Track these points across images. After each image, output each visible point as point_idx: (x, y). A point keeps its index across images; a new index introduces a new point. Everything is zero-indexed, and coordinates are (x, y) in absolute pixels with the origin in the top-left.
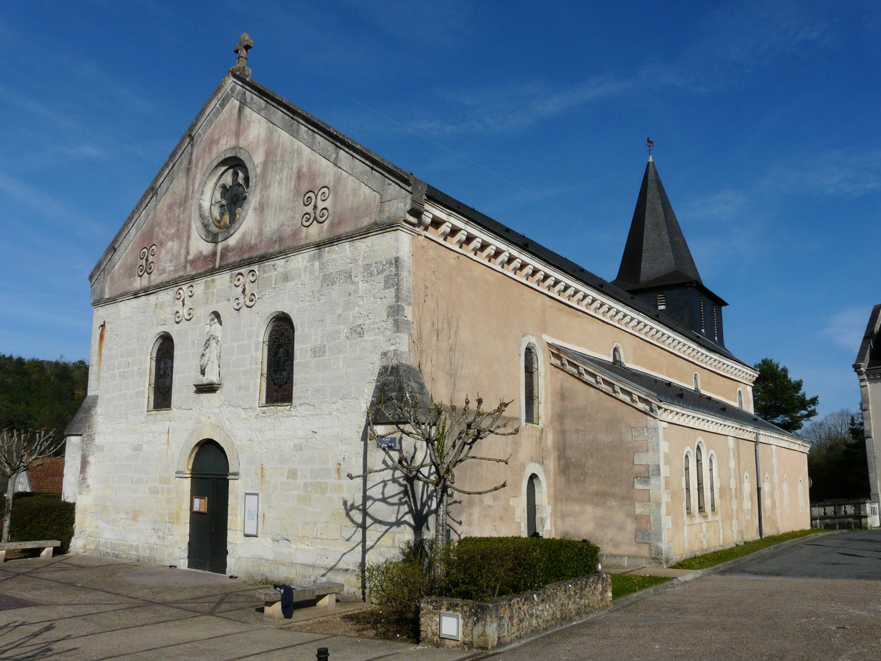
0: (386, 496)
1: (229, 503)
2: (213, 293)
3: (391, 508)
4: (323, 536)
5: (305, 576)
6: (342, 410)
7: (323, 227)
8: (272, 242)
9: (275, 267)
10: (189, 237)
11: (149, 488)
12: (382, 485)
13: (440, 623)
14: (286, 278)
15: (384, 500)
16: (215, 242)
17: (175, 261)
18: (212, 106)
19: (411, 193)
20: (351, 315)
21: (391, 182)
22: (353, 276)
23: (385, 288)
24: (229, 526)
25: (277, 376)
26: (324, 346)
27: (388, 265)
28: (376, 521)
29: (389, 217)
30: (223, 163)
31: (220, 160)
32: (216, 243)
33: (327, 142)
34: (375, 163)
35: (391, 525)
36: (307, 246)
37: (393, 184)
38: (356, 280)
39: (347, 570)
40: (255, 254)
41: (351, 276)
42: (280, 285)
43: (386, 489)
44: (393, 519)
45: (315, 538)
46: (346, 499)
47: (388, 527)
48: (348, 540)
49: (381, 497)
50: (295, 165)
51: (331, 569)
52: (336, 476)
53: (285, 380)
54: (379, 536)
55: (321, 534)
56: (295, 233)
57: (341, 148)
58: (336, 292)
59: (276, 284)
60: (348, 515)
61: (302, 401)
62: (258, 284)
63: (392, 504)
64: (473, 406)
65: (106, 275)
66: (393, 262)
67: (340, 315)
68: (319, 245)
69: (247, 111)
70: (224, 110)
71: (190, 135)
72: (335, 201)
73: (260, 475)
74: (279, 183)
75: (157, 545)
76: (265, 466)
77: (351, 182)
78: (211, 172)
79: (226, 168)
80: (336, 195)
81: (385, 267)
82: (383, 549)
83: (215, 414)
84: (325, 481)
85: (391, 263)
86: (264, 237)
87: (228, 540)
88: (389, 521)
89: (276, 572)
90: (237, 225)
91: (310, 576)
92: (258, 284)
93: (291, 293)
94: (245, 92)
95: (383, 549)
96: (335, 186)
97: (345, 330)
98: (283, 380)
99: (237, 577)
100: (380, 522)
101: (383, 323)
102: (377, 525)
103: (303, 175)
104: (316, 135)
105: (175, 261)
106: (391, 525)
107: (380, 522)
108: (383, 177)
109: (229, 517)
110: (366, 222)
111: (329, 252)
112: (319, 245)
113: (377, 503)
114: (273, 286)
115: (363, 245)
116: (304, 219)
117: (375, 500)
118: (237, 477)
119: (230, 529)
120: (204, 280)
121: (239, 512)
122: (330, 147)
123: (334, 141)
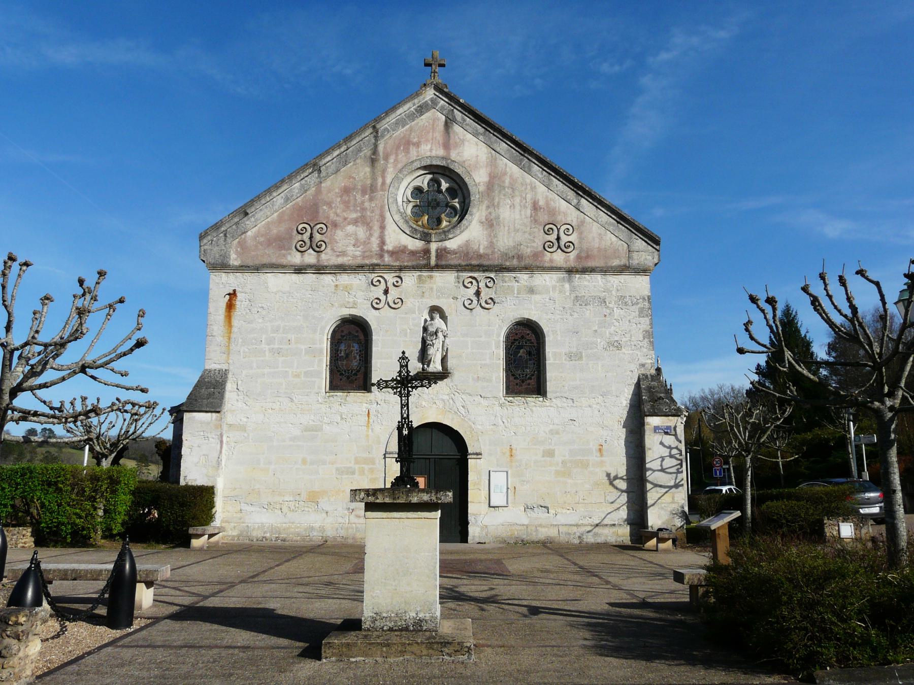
0: (664, 467)
1: (470, 479)
2: (432, 289)
3: (670, 476)
4: (586, 501)
5: (569, 534)
6: (603, 404)
7: (569, 256)
8: (505, 255)
9: (517, 279)
10: (383, 228)
11: (337, 469)
12: (661, 459)
13: (839, 530)
14: (531, 291)
15: (663, 470)
16: (426, 238)
17: (362, 247)
18: (406, 107)
19: (658, 251)
20: (607, 332)
21: (637, 237)
22: (607, 303)
23: (640, 316)
24: (469, 499)
25: (519, 372)
26: (581, 353)
27: (641, 300)
28: (656, 485)
29: (638, 264)
30: (424, 168)
31: (424, 164)
32: (429, 242)
33: (566, 187)
34: (621, 218)
35: (671, 487)
36: (558, 269)
37: (640, 240)
38: (611, 306)
39: (614, 525)
40: (486, 263)
41: (605, 302)
42: (524, 296)
43: (664, 463)
44: (672, 483)
45: (576, 503)
46: (609, 472)
47: (667, 489)
48: (612, 503)
49: (660, 468)
50: (529, 196)
51: (597, 525)
52: (598, 454)
53: (528, 376)
54: (659, 496)
55: (584, 499)
56: (536, 255)
57: (582, 197)
58: (590, 312)
59: (518, 294)
60: (611, 483)
61: (555, 395)
62: (496, 290)
63: (671, 473)
64: (67, 406)
65: (229, 240)
66: (647, 298)
67: (596, 331)
68: (570, 271)
69: (457, 128)
70: (422, 117)
71: (374, 127)
72: (581, 238)
73: (508, 454)
74: (510, 207)
75: (355, 524)
76: (514, 447)
77: (595, 229)
78: (410, 172)
79: (426, 172)
80: (581, 233)
81: (638, 301)
82: (663, 505)
83: (443, 400)
84: (586, 458)
85: (644, 299)
86: (496, 250)
87: (469, 512)
88: (669, 485)
89: (534, 533)
90: (458, 232)
91: (575, 533)
92: (496, 290)
93: (538, 305)
94: (453, 110)
95: (663, 505)
96: (578, 226)
97: (601, 343)
98: (352, 372)
99: (485, 543)
100: (661, 486)
101: (639, 342)
102: (658, 489)
103: (541, 208)
104: (552, 178)
105: (362, 247)
106: (671, 487)
107: (661, 486)
108: (629, 232)
109: (469, 492)
110: (616, 263)
111: (579, 278)
112: (570, 271)
113: (656, 472)
114: (515, 295)
115: (615, 280)
116: (569, 250)
117: (654, 471)
118: (479, 456)
119: (471, 502)
120: (416, 274)
121: (483, 487)
122: (571, 194)
123: (575, 189)
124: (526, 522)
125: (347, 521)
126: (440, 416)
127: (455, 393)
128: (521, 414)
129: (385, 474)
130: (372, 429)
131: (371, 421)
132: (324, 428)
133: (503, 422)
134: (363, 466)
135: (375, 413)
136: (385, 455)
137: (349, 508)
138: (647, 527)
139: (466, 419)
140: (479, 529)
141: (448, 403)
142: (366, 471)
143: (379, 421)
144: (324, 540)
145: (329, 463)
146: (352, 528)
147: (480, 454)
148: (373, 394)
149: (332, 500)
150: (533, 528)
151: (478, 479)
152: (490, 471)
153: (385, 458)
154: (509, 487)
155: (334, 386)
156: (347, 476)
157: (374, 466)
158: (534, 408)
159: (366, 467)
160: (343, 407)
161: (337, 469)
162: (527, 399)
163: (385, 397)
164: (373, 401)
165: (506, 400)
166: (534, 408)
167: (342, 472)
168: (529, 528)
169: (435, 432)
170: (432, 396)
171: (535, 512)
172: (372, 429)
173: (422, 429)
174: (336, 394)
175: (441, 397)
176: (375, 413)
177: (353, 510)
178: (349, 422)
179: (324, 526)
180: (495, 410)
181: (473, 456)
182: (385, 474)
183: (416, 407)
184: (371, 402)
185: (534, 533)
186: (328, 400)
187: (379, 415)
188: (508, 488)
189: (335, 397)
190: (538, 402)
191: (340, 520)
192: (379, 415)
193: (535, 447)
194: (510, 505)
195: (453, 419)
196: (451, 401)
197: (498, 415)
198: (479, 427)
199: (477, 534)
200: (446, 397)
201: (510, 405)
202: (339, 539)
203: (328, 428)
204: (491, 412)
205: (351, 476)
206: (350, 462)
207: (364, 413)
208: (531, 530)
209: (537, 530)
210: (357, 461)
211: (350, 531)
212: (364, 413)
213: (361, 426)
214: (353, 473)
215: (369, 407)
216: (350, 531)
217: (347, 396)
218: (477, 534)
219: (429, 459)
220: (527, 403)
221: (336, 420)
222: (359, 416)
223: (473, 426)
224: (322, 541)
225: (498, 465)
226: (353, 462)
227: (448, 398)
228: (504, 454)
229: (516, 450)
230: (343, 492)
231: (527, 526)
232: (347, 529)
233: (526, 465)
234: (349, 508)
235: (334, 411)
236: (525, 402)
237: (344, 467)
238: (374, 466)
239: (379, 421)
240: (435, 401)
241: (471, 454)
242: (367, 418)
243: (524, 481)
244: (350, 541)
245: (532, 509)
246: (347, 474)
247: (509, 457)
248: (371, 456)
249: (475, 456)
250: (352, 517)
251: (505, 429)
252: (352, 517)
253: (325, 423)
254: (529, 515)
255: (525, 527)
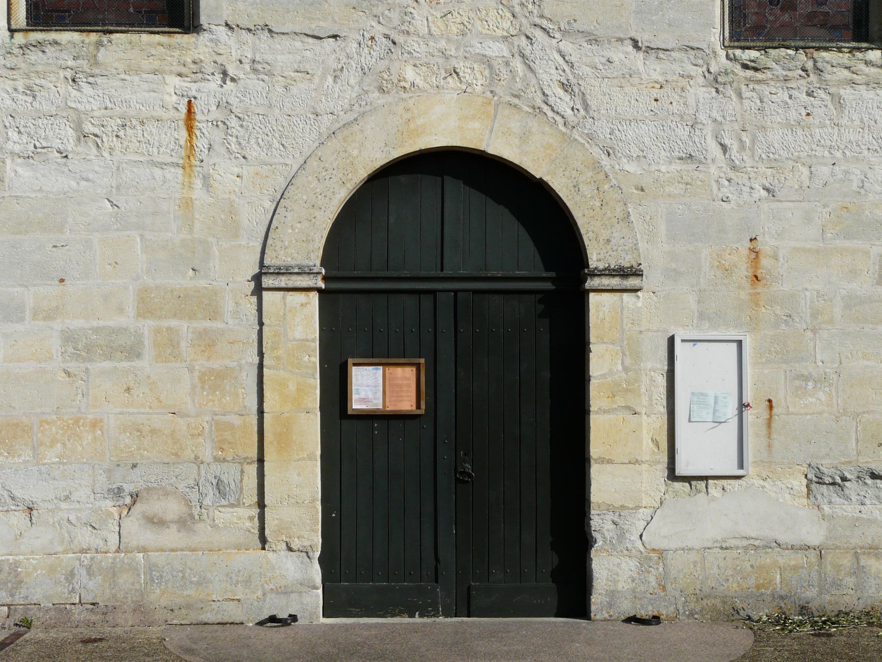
11: (68, 337)
73: (743, 271)
76: (766, 244)
83: (486, 61)
118: (632, 282)
119: (602, 461)
121: (645, 400)
124: (815, 535)
125: (113, 540)
126: (477, 125)
127: (530, 31)
128: (793, 115)
129: (261, 354)
130: (206, 178)
131: (201, 143)
132: (9, 173)
133: (724, 148)
134: (173, 323)
135: (215, 114)
136: (257, 279)
137: (120, 489)
138: (588, 266)
139: (576, 135)
140: (633, 564)
141: (504, 74)
142: (183, 345)
143: (234, 147)
144: (18, 617)
145: (35, 316)
146: (133, 569)
147: (637, 273)
148: (204, 37)
149: (51, 456)
150: (847, 561)
151: (626, 369)
152: (671, 341)
153: (258, 290)
154: (748, 398)
155: (741, 340)
156: (107, 365)
157: (218, 325)
158: (846, 93)
159: (183, 326)
160: (87, 89)
161: (68, 337)
162: (816, 54)
163: (255, 50)
164: (209, 68)
165: (734, 59)
166: (846, 93)
167: (89, 349)
168: (829, 558)
169: (455, 189)
170: (443, 44)
171: (848, 498)
172: (206, 178)
173: (403, 179)
174: (53, 36)
175: (478, 49)
176: (215, 114)
177: (135, 497)
178: (111, 149)
179: (17, 564)
180: (691, 101)
181: (606, 282)
182: (261, 354)
183: (381, 90)
184: (198, 71)
185: (850, 581)
186: (18, 61)
187: (233, 122)
188: (743, 406)
189: (49, 50)
190: (862, 66)
191: (85, 537)
192: (233, 122)
193: (847, 244)
194: (751, 469)
195: (524, 137)
196: (518, 65)
197: (702, 117)
198: (631, 167)
199: (623, 585)
200: (496, 50)
201: (750, 80)
202: (79, 614)
203: (25, 172)
204: (675, 108)
205: (125, 364)
206: (121, 310)
207: (172, 113)
208: (838, 568)
209: (859, 571)
210: (145, 309)
211: (124, 579)
212: (172, 113)
213: (162, 165)
214: (133, 352)
215: (193, 89)
216: (124, 579)
217: (99, 44)
218: (623, 585)
219: (433, 292)
220: (819, 70)
221: (57, 144)
222: (151, 127)
223: (605, 161)
224: (10, 622)
225: (702, 316)
226: (131, 311)
227: (506, 53)
228: (728, 271)
229: (776, 257)
230: (94, 425)
231: (820, 551)
232: (112, 573)
233: (815, 314)
234: (120, 489)
235: (46, 108)
236: (810, 65)
237: (96, 330)
238: (218, 325)
239: (234, 147)
240: (454, 63)
241: (601, 273)
242: (184, 134)
243: (806, 378)
244: (125, 622)
245: (839, 483)
246: (109, 357)
247: (746, 284)
248: (202, 283)
249: (615, 282)
250: (133, 526)
251: (732, 175)
252: (133, 526)
253: (12, 153)
254: (826, 508)
255: (813, 556)
